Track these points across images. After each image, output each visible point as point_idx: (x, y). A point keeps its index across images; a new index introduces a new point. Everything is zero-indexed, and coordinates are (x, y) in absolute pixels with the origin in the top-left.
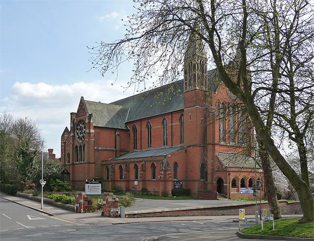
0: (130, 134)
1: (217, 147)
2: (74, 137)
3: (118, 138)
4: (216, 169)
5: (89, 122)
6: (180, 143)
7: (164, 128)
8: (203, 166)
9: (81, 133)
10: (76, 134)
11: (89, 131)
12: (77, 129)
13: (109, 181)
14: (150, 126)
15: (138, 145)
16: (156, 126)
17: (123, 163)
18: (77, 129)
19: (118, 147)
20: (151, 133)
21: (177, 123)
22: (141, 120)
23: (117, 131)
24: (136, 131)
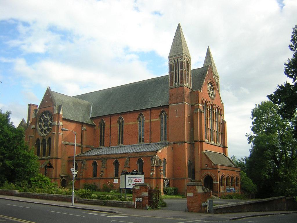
0: (95, 130)
1: (204, 143)
2: (35, 129)
3: (84, 132)
4: (204, 167)
5: (59, 114)
6: (160, 140)
7: (140, 125)
8: (192, 164)
9: (44, 126)
10: (38, 126)
11: (58, 123)
12: (40, 121)
13: (153, 178)
14: (122, 122)
15: (106, 141)
16: (130, 122)
17: (98, 159)
18: (40, 121)
19: (84, 143)
20: (122, 129)
21: (157, 120)
22: (111, 115)
23: (84, 125)
24: (104, 126)
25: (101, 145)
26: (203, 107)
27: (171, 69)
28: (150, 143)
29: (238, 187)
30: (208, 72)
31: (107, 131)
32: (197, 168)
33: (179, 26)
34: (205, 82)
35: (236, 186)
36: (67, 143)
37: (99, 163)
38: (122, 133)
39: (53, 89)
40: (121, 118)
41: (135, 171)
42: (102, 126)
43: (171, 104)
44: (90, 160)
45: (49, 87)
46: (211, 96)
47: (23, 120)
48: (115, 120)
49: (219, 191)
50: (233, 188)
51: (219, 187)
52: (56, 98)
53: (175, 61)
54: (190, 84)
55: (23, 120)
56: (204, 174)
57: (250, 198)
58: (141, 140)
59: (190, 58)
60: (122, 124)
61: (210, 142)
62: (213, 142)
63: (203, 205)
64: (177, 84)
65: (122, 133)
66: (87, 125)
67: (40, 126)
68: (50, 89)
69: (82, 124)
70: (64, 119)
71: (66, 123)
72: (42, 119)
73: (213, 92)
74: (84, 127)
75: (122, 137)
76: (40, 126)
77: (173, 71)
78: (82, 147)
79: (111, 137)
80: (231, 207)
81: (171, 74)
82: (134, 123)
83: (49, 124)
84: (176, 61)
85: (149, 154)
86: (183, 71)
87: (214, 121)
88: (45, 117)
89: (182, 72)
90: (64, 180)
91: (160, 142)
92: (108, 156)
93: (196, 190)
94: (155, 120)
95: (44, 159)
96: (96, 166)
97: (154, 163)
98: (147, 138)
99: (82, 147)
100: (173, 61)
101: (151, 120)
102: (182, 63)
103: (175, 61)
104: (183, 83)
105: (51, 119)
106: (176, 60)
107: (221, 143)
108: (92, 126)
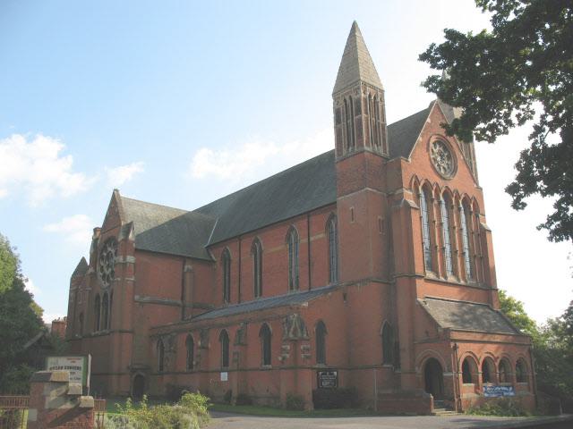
1: (420, 283)
3: (188, 277)
5: (126, 239)
8: (389, 332)
9: (108, 266)
10: (98, 268)
11: (125, 259)
12: (102, 258)
18: (102, 258)
21: (321, 236)
22: (239, 237)
29: (526, 383)
30: (431, 118)
31: (234, 273)
33: (354, 27)
34: (420, 139)
38: (261, 275)
39: (122, 194)
40: (257, 240)
42: (226, 261)
43: (340, 196)
45: (117, 190)
46: (438, 170)
47: (83, 260)
50: (508, 387)
53: (345, 101)
54: (384, 144)
57: (561, 410)
59: (382, 91)
61: (442, 279)
65: (261, 275)
66: (194, 260)
68: (119, 195)
69: (184, 259)
70: (137, 251)
71: (145, 259)
73: (449, 163)
75: (261, 280)
77: (343, 123)
84: (348, 101)
86: (361, 118)
87: (454, 228)
88: (109, 249)
89: (360, 120)
90: (139, 376)
91: (328, 286)
94: (319, 236)
97: (289, 331)
100: (342, 101)
101: (312, 239)
102: (358, 101)
103: (345, 101)
104: (363, 146)
106: (347, 98)
107: (460, 277)
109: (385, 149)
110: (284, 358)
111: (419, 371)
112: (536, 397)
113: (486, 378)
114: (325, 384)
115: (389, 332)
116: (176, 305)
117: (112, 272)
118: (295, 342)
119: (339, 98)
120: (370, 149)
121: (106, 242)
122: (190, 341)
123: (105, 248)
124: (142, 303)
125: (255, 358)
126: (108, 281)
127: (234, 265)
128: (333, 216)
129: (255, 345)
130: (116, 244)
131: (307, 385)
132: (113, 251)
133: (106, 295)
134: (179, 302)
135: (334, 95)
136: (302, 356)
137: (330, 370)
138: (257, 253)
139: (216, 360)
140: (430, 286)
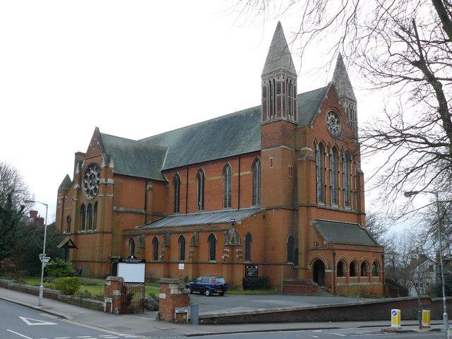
2: (79, 190)
3: (150, 194)
4: (312, 246)
5: (107, 167)
8: (292, 241)
9: (91, 184)
10: (83, 184)
12: (86, 177)
15: (182, 206)
16: (213, 177)
17: (159, 234)
18: (86, 177)
19: (149, 209)
21: (248, 173)
22: (188, 167)
25: (175, 212)
26: (316, 151)
27: (264, 95)
28: (239, 208)
31: (183, 192)
32: (302, 247)
35: (362, 276)
36: (121, 209)
37: (161, 239)
39: (102, 131)
40: (201, 171)
41: (132, 257)
42: (177, 183)
44: (149, 234)
47: (67, 177)
48: (193, 174)
49: (332, 284)
51: (332, 277)
52: (107, 143)
55: (67, 177)
56: (313, 256)
58: (228, 204)
60: (203, 179)
61: (328, 207)
62: (335, 206)
63: (177, 311)
64: (272, 117)
66: (154, 181)
67: (86, 185)
70: (115, 175)
72: (88, 175)
74: (149, 186)
76: (86, 185)
78: (146, 215)
79: (189, 199)
80: (263, 314)
81: (264, 103)
82: (217, 178)
83: (96, 181)
85: (223, 227)
88: (92, 172)
89: (280, 97)
91: (252, 208)
92: (172, 230)
93: (169, 290)
94: (246, 173)
95: (89, 233)
96: (215, 241)
98: (234, 201)
99: (146, 215)
100: (267, 82)
105: (99, 175)
108: (165, 183)
109: (295, 118)
110: (225, 257)
111: (310, 267)
112: (384, 287)
113: (353, 273)
114: (250, 274)
115: (292, 241)
116: (141, 214)
117: (95, 189)
118: (232, 247)
119: (266, 79)
120: (285, 119)
121: (89, 166)
122: (155, 241)
123: (88, 171)
124: (118, 212)
125: (204, 256)
126: (91, 194)
127: (183, 187)
128: (257, 160)
129: (205, 247)
130: (98, 168)
131: (239, 275)
132: (96, 174)
133: (90, 205)
134: (143, 211)
135: (263, 76)
136: (237, 256)
137: (253, 265)
138: (201, 179)
139: (175, 255)
140: (321, 212)
